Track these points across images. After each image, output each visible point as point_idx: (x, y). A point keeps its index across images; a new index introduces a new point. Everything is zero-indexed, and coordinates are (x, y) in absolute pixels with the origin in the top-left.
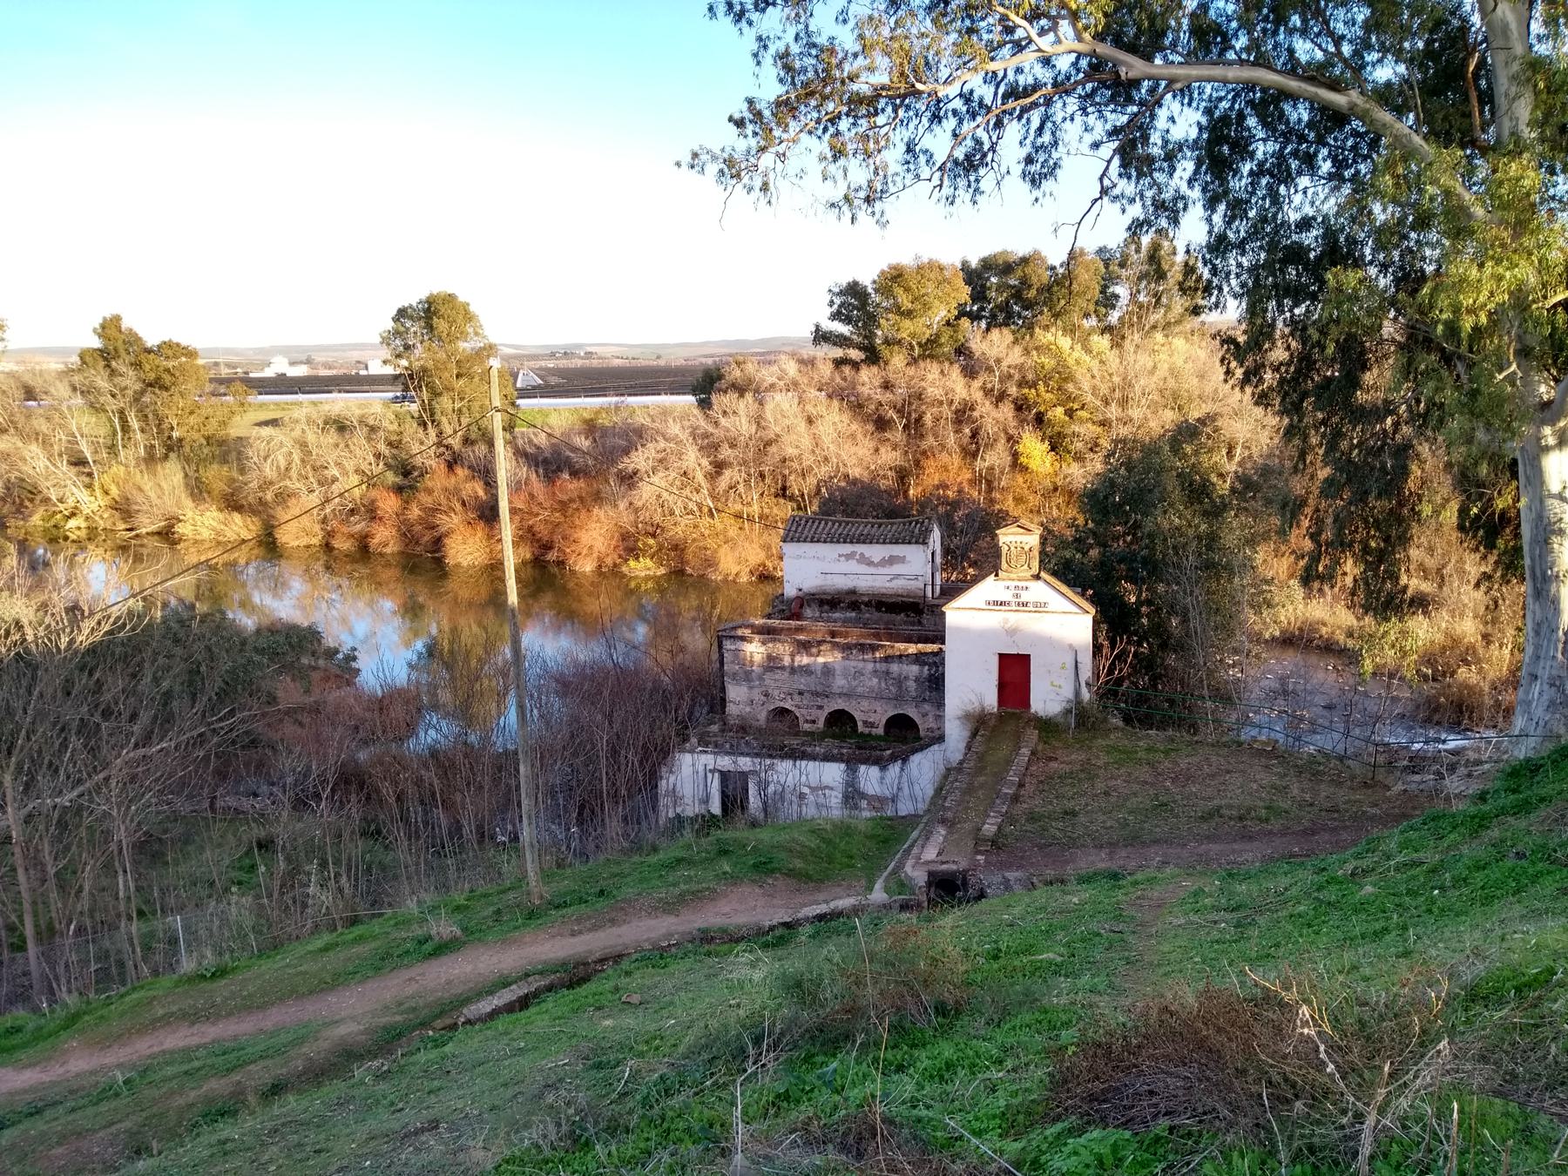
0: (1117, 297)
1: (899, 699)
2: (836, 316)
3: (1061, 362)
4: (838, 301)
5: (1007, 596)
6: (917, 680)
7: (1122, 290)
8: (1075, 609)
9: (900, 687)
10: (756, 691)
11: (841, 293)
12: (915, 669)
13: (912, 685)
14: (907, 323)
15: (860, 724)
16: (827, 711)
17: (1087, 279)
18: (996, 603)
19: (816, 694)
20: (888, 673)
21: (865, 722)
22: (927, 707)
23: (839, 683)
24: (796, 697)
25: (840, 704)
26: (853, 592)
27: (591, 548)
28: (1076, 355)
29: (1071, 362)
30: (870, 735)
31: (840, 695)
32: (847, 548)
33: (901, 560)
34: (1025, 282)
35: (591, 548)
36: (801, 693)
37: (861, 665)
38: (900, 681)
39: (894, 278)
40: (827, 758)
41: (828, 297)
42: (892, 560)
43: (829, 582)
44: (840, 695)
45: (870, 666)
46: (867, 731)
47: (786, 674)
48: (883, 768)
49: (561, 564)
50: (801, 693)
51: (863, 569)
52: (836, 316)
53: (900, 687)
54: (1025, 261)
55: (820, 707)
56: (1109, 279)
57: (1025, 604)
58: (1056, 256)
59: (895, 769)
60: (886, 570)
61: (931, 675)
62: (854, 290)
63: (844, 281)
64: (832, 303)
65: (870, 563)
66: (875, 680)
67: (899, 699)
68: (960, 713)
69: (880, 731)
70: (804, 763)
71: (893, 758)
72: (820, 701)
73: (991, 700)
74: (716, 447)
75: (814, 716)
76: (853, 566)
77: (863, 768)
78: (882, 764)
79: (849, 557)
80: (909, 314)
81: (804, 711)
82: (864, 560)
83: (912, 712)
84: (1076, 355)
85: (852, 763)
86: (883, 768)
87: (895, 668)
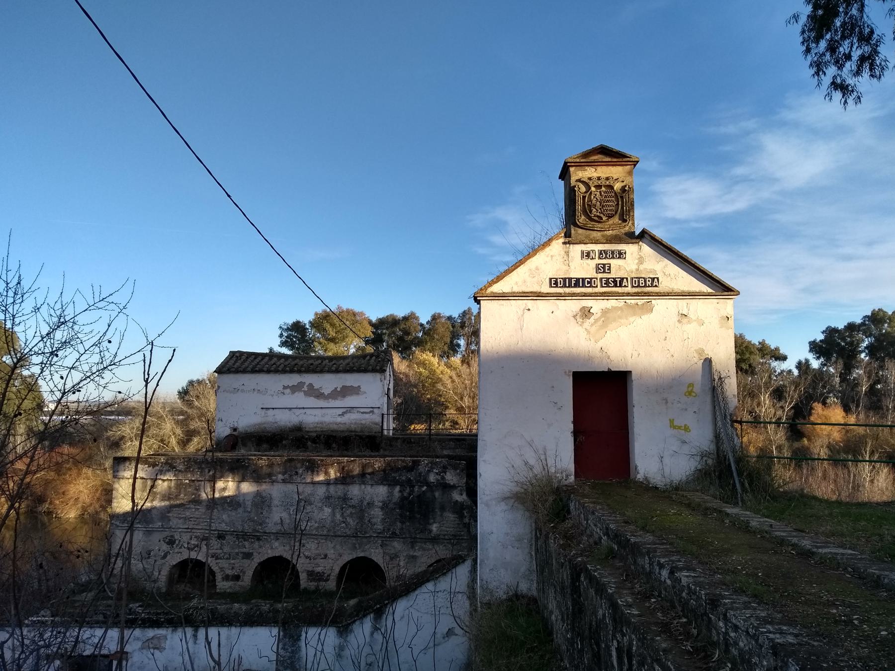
0: (459, 346)
1: (359, 535)
2: (283, 344)
3: (432, 372)
4: (285, 334)
5: (584, 269)
6: (385, 506)
7: (462, 342)
8: (705, 289)
9: (361, 518)
10: (157, 537)
11: (288, 329)
12: (382, 491)
13: (377, 514)
14: (331, 346)
15: (303, 576)
16: (257, 559)
17: (443, 331)
18: (568, 282)
19: (243, 536)
20: (345, 499)
21: (312, 575)
22: (397, 545)
23: (277, 516)
24: (215, 543)
25: (278, 549)
26: (298, 429)
27: (77, 499)
28: (441, 368)
29: (438, 372)
30: (317, 590)
31: (278, 535)
32: (294, 379)
33: (354, 391)
34: (407, 333)
35: (77, 499)
36: (221, 537)
37: (309, 489)
38: (362, 509)
39: (322, 321)
40: (251, 621)
41: (279, 332)
42: (346, 391)
43: (270, 419)
44: (278, 535)
45: (321, 491)
46: (312, 585)
47: (202, 509)
48: (344, 630)
49: (49, 513)
50: (221, 537)
51: (312, 402)
52: (283, 344)
53: (361, 518)
54: (405, 319)
55: (248, 556)
56: (455, 336)
57: (618, 282)
58: (424, 318)
59: (363, 630)
60: (338, 403)
61: (403, 499)
62: (297, 327)
63: (290, 321)
64: (281, 336)
65: (319, 395)
66: (328, 510)
67: (359, 535)
68: (509, 487)
69: (331, 585)
70: (213, 632)
71: (360, 613)
72: (247, 546)
73: (561, 456)
74: (188, 418)
75: (233, 568)
76: (299, 399)
77: (312, 633)
78: (343, 624)
79: (295, 389)
80: (333, 340)
81: (223, 563)
82: (314, 393)
83: (376, 555)
84: (441, 368)
85: (290, 627)
86: (344, 630)
87: (355, 491)
